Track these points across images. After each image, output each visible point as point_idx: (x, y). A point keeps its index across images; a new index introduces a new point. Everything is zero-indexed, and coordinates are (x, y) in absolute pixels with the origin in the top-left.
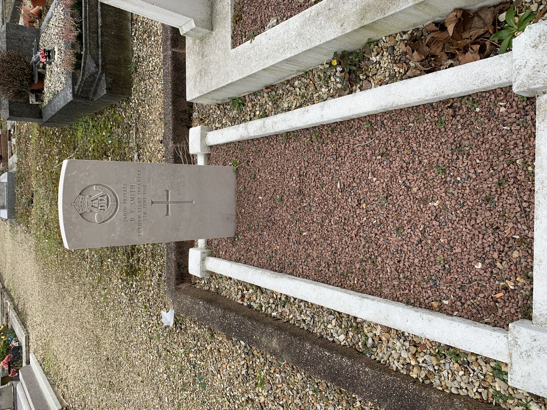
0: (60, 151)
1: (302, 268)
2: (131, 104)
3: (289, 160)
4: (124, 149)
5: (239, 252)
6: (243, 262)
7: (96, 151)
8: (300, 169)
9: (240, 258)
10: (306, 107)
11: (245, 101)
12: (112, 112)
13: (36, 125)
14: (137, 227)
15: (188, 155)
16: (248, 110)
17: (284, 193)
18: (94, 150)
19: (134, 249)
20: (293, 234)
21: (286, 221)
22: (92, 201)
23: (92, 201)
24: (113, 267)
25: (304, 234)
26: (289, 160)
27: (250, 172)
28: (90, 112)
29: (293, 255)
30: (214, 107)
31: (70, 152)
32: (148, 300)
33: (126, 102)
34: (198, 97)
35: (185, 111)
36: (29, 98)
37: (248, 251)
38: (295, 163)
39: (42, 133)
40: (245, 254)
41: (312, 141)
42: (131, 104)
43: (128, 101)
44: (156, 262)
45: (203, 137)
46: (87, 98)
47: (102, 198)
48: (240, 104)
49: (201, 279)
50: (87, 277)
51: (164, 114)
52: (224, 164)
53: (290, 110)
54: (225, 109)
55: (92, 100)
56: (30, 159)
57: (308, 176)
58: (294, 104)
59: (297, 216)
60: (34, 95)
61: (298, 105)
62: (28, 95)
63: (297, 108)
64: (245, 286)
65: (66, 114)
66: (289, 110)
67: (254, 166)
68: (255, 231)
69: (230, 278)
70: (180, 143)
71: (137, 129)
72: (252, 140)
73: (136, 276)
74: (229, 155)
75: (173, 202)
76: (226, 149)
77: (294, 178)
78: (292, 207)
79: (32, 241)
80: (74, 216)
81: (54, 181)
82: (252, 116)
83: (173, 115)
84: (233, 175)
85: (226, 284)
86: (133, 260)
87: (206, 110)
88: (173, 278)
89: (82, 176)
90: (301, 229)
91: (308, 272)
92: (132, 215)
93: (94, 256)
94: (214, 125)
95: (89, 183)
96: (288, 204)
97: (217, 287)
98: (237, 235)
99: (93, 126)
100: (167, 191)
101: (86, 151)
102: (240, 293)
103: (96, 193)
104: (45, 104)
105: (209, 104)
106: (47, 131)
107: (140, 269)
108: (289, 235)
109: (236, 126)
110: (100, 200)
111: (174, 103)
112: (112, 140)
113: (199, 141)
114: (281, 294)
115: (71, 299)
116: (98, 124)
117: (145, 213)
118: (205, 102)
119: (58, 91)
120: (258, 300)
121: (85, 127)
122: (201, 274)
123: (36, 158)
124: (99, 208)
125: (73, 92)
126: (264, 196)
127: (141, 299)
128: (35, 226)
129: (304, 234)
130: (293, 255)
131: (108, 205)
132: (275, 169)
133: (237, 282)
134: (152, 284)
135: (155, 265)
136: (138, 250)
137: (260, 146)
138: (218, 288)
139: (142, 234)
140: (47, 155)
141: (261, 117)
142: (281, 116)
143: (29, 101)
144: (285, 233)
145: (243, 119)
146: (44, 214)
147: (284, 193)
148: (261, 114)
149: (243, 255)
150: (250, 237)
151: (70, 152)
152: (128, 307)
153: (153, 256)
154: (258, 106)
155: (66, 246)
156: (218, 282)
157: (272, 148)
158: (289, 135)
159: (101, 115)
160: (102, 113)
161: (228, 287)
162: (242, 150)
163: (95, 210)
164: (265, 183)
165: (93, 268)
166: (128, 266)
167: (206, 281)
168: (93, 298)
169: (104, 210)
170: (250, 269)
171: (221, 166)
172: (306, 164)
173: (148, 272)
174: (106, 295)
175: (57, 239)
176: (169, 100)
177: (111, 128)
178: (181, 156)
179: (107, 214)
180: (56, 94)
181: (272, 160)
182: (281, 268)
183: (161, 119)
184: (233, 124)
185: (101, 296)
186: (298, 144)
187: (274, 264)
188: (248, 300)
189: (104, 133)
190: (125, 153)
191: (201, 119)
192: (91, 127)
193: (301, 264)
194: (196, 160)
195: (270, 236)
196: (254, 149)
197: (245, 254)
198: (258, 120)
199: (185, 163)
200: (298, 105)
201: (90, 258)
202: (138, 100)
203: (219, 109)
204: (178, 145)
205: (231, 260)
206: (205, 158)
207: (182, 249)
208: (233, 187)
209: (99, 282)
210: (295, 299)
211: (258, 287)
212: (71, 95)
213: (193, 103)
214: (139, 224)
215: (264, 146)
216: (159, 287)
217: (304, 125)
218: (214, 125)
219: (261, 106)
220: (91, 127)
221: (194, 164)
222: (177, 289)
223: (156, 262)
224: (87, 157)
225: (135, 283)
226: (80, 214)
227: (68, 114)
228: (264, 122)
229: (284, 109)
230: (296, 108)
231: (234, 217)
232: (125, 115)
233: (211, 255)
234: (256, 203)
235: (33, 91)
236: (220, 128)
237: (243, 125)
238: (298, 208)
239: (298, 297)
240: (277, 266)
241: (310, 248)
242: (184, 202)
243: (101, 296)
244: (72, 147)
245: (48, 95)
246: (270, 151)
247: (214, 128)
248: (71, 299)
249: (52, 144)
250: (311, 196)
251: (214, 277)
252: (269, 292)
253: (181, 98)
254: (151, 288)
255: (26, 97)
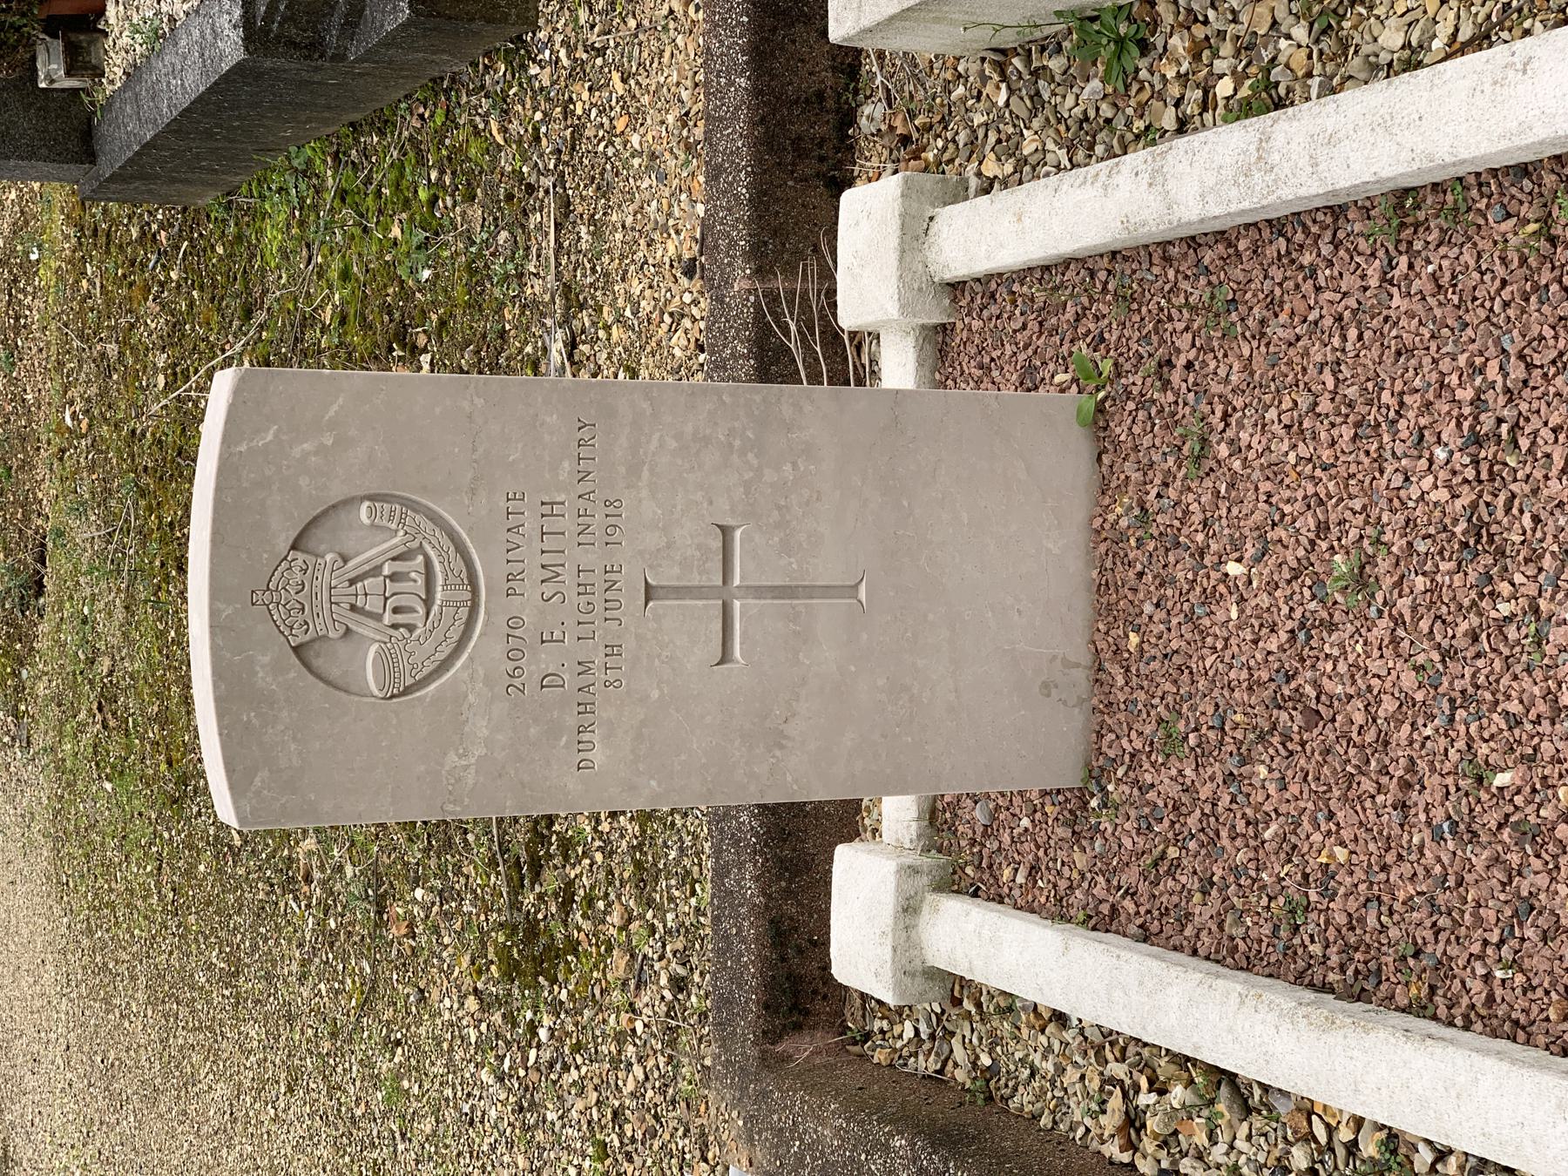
0: (176, 326)
1: (1488, 978)
2: (534, 70)
3: (1410, 352)
4: (499, 310)
5: (1109, 873)
6: (1133, 929)
7: (354, 325)
8: (1478, 401)
9: (1113, 908)
10: (1520, 45)
11: (1155, 23)
12: (439, 120)
13: (60, 194)
14: (571, 720)
15: (833, 336)
16: (1170, 74)
17: (1377, 542)
18: (343, 321)
19: (544, 840)
20: (1432, 781)
21: (1389, 705)
22: (352, 582)
23: (352, 582)
24: (436, 930)
25: (1501, 779)
26: (1410, 352)
27: (1172, 422)
28: (326, 122)
29: (1432, 901)
30: (974, 67)
31: (224, 328)
32: (615, 1114)
33: (509, 63)
34: (892, 18)
35: (820, 95)
36: (34, 59)
37: (1161, 867)
38: (1445, 365)
39: (92, 237)
40: (1143, 887)
41: (1553, 240)
42: (534, 70)
43: (520, 54)
44: (661, 911)
45: (914, 232)
46: (314, 48)
47: (400, 566)
48: (1120, 42)
49: (899, 1011)
50: (302, 978)
51: (709, 119)
52: (1029, 381)
53: (1419, 65)
54: (1035, 74)
55: (340, 57)
56: (31, 372)
57: (1524, 443)
58: (1444, 30)
59: (1460, 677)
60: (58, 46)
61: (1466, 33)
62: (30, 46)
63: (1462, 51)
64: (1146, 1066)
65: (209, 134)
66: (1412, 65)
67: (1199, 390)
68: (1201, 757)
69: (1060, 1018)
70: (790, 270)
71: (566, 205)
72: (1192, 242)
73: (553, 981)
74: (1054, 330)
75: (759, 592)
76: (1040, 297)
77: (1440, 454)
78: (1424, 625)
79: (40, 790)
80: (266, 659)
81: (145, 480)
82: (1191, 109)
83: (753, 124)
84: (1079, 446)
85: (1035, 1048)
86: (540, 897)
87: (934, 85)
88: (749, 998)
89: (305, 455)
90: (1483, 749)
91: (1522, 1003)
92: (545, 660)
93: (340, 869)
94: (972, 167)
95: (337, 493)
96: (1403, 605)
97: (986, 1060)
98: (1096, 775)
99: (342, 195)
100: (726, 531)
101: (303, 326)
102: (1116, 1102)
103: (371, 539)
104: (109, 89)
105: (951, 53)
106: (115, 222)
107: (573, 947)
108: (1406, 786)
109: (1095, 168)
110: (393, 577)
111: (761, 55)
112: (435, 262)
113: (892, 258)
114: (1359, 1122)
115: (222, 1089)
116: (368, 181)
117: (612, 650)
118: (925, 42)
119: (172, 19)
120: (1222, 1148)
121: (302, 200)
122: (898, 986)
123: (61, 364)
124: (388, 618)
125: (248, 21)
126: (1258, 560)
127: (580, 1105)
128: (54, 711)
129: (1501, 779)
130: (1432, 901)
131: (428, 602)
132: (1325, 406)
133: (1096, 1038)
134: (639, 1026)
135: (653, 930)
136: (566, 845)
137: (1237, 273)
138: (992, 1072)
139: (597, 756)
140: (112, 349)
141: (1245, 110)
142: (1362, 103)
143: (34, 71)
144: (1384, 771)
145: (1139, 125)
146: (96, 651)
147: (1377, 542)
148: (1244, 92)
149: (1131, 893)
150: (1174, 791)
151: (224, 328)
152: (510, 1145)
153: (644, 877)
154: (1227, 49)
155: (225, 810)
156: (992, 1033)
157: (1307, 287)
158: (1408, 209)
159: (382, 133)
160: (383, 125)
161: (1048, 1066)
162: (1126, 299)
163: (365, 628)
164: (1265, 486)
165: (334, 934)
166: (514, 929)
167: (923, 1027)
168: (331, 1090)
169: (411, 628)
170: (1175, 971)
171: (1008, 392)
172: (1517, 371)
173: (619, 963)
174: (398, 1077)
175: (157, 777)
176: (735, 44)
177: (433, 201)
178: (797, 342)
179: (423, 650)
180: (162, 36)
181: (1306, 353)
182: (1354, 976)
183: (689, 148)
184: (1080, 155)
185: (376, 1081)
186: (1468, 257)
187: (1315, 949)
188: (1164, 1144)
189: (396, 232)
190: (502, 334)
191: (905, 140)
192: (328, 197)
193: (1481, 957)
194: (873, 361)
195: (1294, 789)
196: (1198, 292)
197: (1143, 887)
198: (1224, 130)
199: (815, 378)
200: (1463, 36)
201: (323, 883)
202: (571, 50)
203: (1004, 77)
204: (780, 284)
205: (1064, 918)
206: (921, 350)
207: (795, 846)
208: (1077, 504)
209: (366, 1005)
210: (1442, 1154)
211: (1222, 1077)
212: (236, 36)
213: (858, 52)
214: (585, 708)
215: (1257, 273)
216: (672, 1043)
217: (1504, 145)
218: (972, 167)
219: (1247, 48)
220: (328, 197)
221: (860, 382)
222: (771, 1063)
223: (661, 911)
224: (308, 356)
225: (547, 1021)
226: (296, 649)
227: (221, 131)
228: (1265, 139)
229: (1384, 58)
230: (1456, 49)
231: (1081, 677)
232: (504, 130)
233: (952, 883)
234: (1209, 597)
235: (53, 26)
236: (1005, 184)
237: (1137, 158)
238: (1464, 626)
239: (1460, 1145)
240: (1335, 960)
241: (1537, 864)
242: (811, 591)
243: (376, 1081)
244: (234, 305)
245: (125, 40)
246: (1293, 302)
247: (974, 183)
248: (222, 1089)
249: (136, 293)
250: (1547, 562)
251: (968, 1005)
252: (1283, 1108)
253: (799, 28)
254: (630, 1050)
255: (22, 54)
